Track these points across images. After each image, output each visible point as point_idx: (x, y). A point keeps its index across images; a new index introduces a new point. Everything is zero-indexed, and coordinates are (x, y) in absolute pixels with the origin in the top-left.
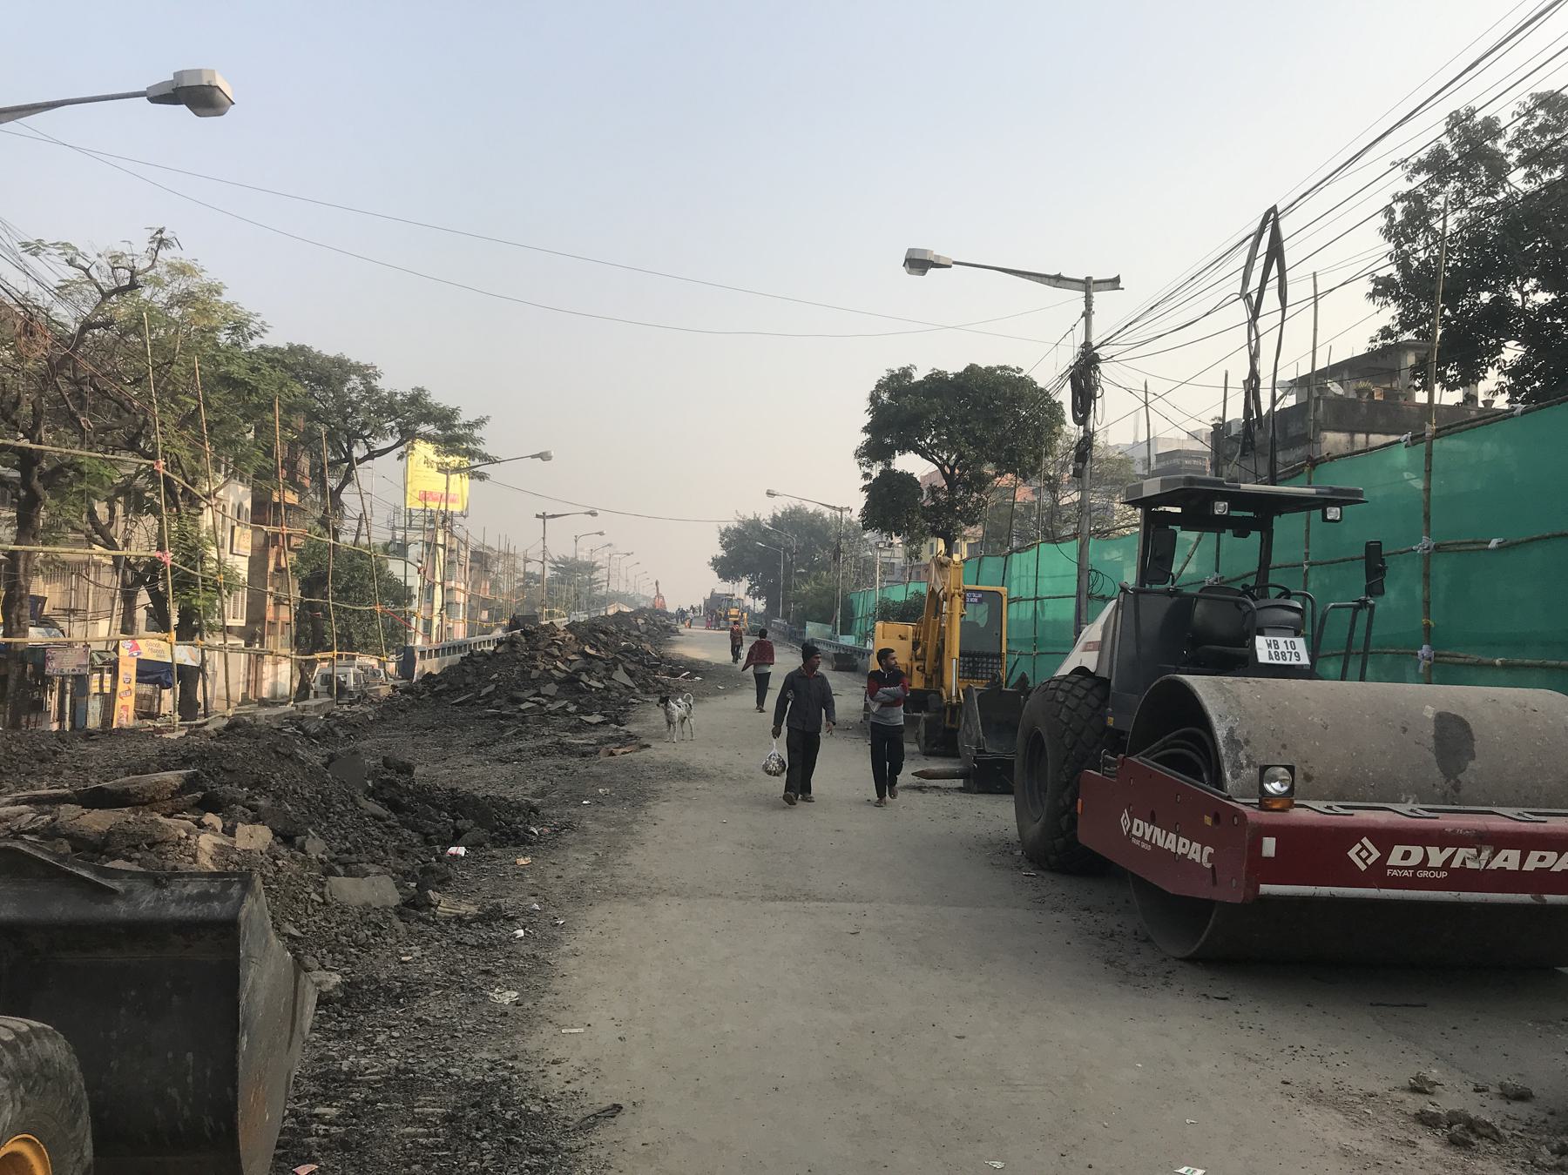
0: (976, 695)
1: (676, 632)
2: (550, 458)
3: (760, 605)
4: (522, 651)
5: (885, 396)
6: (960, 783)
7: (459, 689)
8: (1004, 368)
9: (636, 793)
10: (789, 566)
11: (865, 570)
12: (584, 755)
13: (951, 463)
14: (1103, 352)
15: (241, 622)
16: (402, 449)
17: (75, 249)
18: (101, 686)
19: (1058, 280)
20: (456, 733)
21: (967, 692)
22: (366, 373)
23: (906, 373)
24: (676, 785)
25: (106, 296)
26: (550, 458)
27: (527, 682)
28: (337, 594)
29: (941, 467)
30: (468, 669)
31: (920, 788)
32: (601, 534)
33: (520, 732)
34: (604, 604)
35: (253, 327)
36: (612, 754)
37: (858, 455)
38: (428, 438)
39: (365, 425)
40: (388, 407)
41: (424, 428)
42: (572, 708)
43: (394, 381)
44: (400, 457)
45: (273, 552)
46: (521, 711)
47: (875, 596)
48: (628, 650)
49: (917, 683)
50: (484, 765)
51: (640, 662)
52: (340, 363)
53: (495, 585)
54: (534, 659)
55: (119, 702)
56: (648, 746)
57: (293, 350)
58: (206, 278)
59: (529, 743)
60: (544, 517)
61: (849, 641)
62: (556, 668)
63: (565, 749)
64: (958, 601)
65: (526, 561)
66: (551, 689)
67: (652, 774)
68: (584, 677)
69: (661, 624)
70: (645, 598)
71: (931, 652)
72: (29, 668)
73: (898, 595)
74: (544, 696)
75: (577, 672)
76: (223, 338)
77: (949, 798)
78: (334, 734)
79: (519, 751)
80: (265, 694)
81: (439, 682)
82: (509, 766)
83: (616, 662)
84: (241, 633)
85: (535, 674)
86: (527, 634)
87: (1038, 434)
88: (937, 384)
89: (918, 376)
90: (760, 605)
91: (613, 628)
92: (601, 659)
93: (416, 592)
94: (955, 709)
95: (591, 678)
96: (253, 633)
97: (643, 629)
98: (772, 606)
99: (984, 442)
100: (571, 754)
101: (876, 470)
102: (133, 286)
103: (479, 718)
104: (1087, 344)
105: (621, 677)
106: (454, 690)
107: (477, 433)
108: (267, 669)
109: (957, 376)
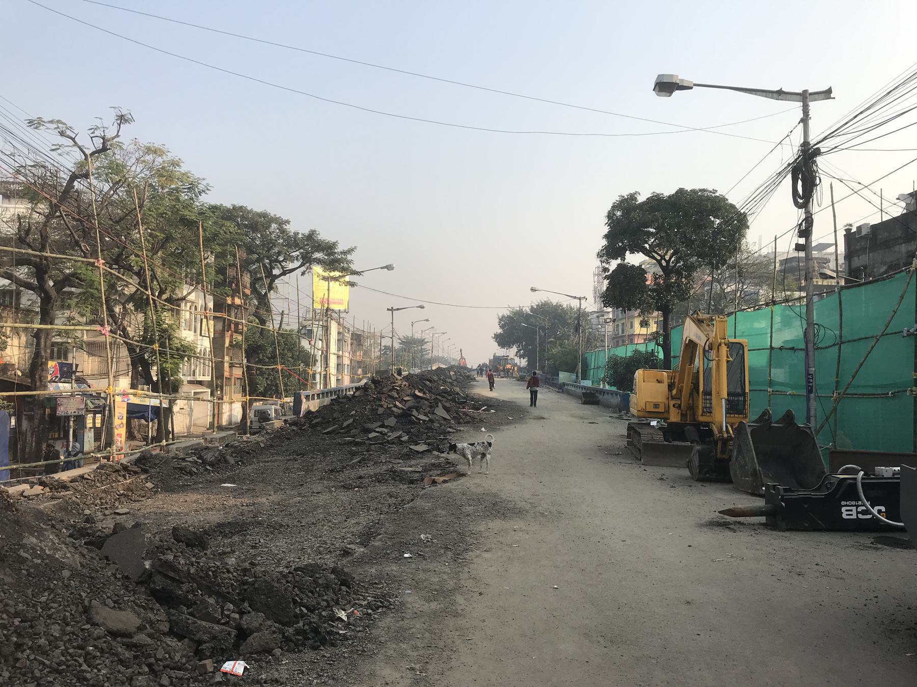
0: (749, 430)
1: (764, 418)
3: (523, 363)
5: (619, 213)
6: (763, 519)
7: (329, 422)
8: (703, 190)
9: (457, 546)
12: (412, 482)
13: (667, 258)
14: (823, 147)
16: (303, 269)
17: (65, 124)
18: (94, 423)
19: (780, 94)
20: (320, 457)
22: (281, 223)
23: (632, 197)
28: (269, 359)
29: (659, 262)
30: (336, 407)
31: (725, 525)
32: (427, 320)
33: (364, 459)
34: (430, 363)
35: (201, 187)
36: (434, 482)
37: (599, 255)
38: (319, 261)
39: (279, 253)
40: (293, 242)
41: (317, 255)
42: (405, 438)
43: (298, 226)
44: (303, 274)
45: (228, 334)
46: (369, 439)
48: (445, 391)
49: (674, 417)
50: (331, 492)
51: (454, 400)
52: (264, 215)
53: (366, 353)
54: (380, 400)
55: (116, 432)
56: (463, 475)
58: (169, 157)
59: (369, 470)
60: (392, 310)
61: (587, 383)
62: (395, 406)
63: (397, 477)
64: (724, 349)
65: (382, 337)
66: (392, 421)
67: (469, 509)
68: (415, 413)
69: (463, 375)
70: (454, 360)
72: (48, 411)
74: (386, 427)
75: (410, 409)
76: (184, 197)
78: (226, 461)
79: (361, 477)
80: (224, 422)
81: (316, 417)
82: (350, 493)
83: (437, 402)
84: (209, 385)
85: (381, 411)
86: (379, 385)
88: (656, 202)
89: (641, 199)
90: (523, 363)
91: (435, 378)
93: (318, 358)
94: (725, 442)
95: (419, 413)
96: (217, 385)
97: (454, 378)
98: (531, 363)
99: (693, 242)
100: (402, 480)
101: (614, 264)
102: (104, 149)
103: (340, 444)
104: (805, 144)
105: (440, 412)
106: (326, 423)
107: (349, 257)
108: (226, 408)
109: (669, 197)
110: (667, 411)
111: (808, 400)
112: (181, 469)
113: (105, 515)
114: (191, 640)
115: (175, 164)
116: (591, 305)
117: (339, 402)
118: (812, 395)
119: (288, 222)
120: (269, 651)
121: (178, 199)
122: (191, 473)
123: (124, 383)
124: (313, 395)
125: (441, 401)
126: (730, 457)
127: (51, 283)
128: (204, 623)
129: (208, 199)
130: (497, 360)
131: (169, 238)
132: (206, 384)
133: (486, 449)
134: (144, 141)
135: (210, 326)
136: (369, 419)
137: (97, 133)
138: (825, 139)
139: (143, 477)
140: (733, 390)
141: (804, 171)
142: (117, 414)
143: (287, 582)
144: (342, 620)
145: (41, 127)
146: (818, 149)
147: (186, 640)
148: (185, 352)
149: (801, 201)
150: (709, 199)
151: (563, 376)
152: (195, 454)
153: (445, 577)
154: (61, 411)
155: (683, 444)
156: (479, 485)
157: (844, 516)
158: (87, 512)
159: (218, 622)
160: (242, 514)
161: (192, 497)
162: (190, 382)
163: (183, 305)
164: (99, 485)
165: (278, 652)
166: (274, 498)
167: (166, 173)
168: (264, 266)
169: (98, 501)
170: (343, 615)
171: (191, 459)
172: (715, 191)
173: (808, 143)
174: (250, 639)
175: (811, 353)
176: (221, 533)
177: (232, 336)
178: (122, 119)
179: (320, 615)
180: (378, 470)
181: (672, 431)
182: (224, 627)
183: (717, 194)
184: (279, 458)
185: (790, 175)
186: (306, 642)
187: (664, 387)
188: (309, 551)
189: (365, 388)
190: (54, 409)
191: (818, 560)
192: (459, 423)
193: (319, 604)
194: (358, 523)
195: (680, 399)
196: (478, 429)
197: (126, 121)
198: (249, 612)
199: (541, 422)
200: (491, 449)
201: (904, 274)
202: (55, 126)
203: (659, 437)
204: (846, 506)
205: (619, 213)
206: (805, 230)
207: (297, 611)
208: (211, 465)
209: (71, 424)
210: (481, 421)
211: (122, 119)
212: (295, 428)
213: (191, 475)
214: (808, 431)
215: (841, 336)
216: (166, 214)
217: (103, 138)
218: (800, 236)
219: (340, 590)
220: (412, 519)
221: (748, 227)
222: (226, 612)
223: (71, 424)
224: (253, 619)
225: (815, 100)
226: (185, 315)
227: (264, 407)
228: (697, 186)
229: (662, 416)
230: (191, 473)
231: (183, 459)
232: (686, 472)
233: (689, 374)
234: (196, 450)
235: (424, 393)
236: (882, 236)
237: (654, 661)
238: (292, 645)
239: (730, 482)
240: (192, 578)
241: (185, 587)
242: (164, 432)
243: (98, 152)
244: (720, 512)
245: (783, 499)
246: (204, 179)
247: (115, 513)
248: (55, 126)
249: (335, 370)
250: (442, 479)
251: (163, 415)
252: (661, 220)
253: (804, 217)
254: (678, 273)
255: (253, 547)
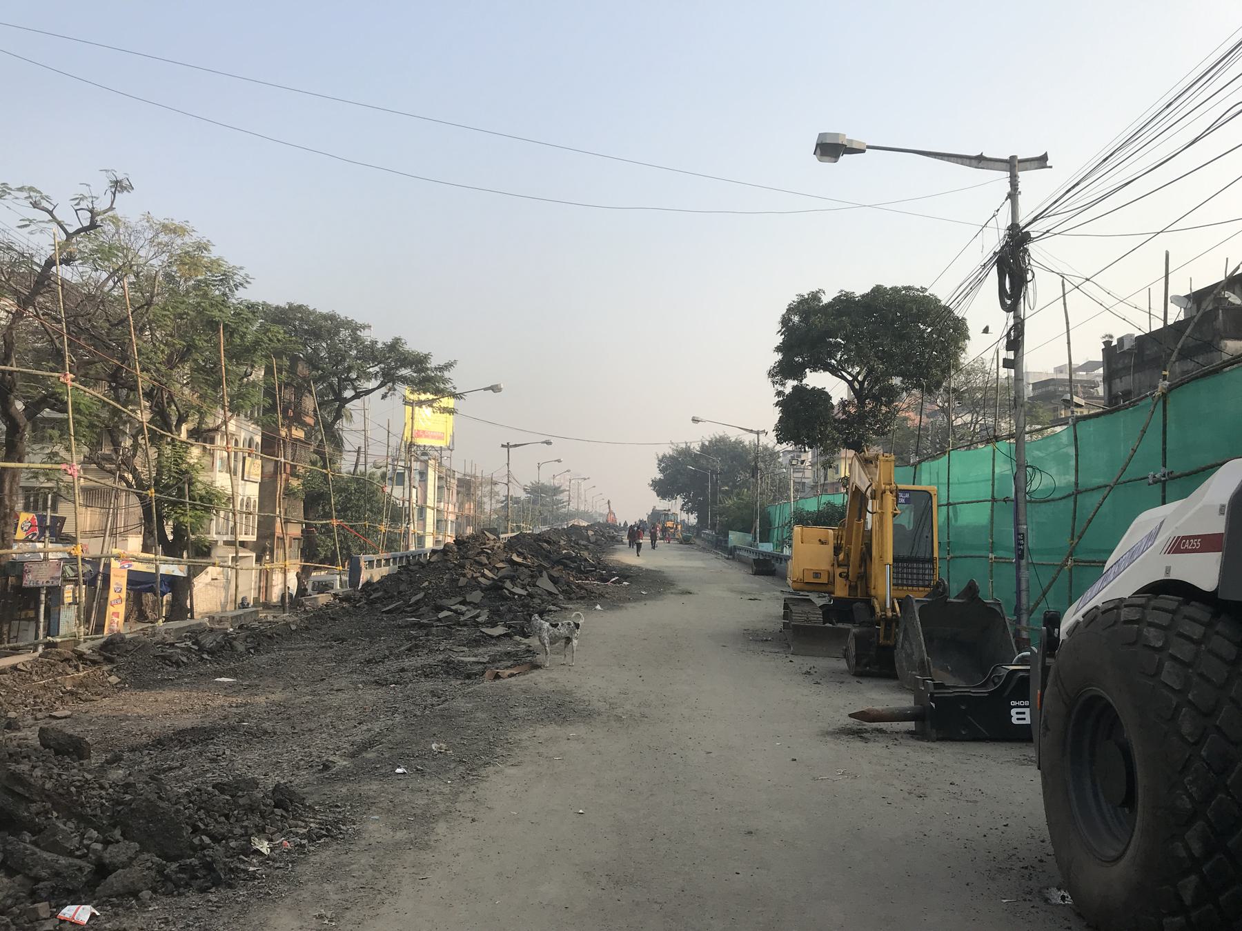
0: (916, 608)
2: (500, 390)
3: (692, 519)
4: (454, 560)
5: (796, 319)
6: (911, 725)
7: (392, 597)
8: (908, 288)
10: (715, 484)
11: (781, 489)
12: (469, 677)
14: (1034, 230)
15: (252, 538)
16: (383, 390)
19: (980, 161)
21: (904, 603)
22: (355, 328)
23: (815, 297)
24: (543, 732)
25: (69, 236)
26: (500, 390)
27: (457, 590)
28: (335, 510)
29: (850, 384)
30: (404, 577)
31: (858, 734)
32: (559, 461)
33: (416, 646)
35: (238, 279)
37: (772, 374)
38: (405, 380)
40: (370, 354)
41: (404, 372)
43: (379, 334)
44: (384, 397)
46: (439, 620)
47: (790, 508)
48: (568, 557)
49: (841, 591)
52: (332, 317)
53: (480, 505)
54: (463, 567)
55: (110, 610)
57: (292, 308)
60: (508, 446)
61: (767, 547)
62: (483, 575)
64: (890, 498)
66: (476, 596)
70: (601, 515)
71: (854, 558)
73: (811, 505)
75: (502, 579)
77: (901, 751)
78: (232, 648)
79: (403, 670)
81: (376, 590)
83: (541, 569)
85: (462, 582)
87: (945, 349)
88: (845, 303)
89: (826, 299)
90: (692, 519)
92: (527, 567)
94: (890, 623)
95: (515, 585)
96: (264, 547)
97: (593, 539)
101: (790, 384)
102: (93, 226)
103: (399, 626)
105: (545, 583)
107: (447, 374)
109: (863, 296)
110: (832, 582)
111: (1018, 568)
112: (164, 658)
113: (36, 719)
114: (27, 876)
115: (202, 247)
116: (770, 440)
117: (413, 569)
118: (1023, 562)
119: (364, 327)
120: (135, 894)
121: (205, 295)
122: (178, 664)
123: (134, 543)
124: (379, 561)
125: (546, 568)
126: (896, 641)
127: (19, 405)
128: (45, 855)
129: (244, 295)
130: (656, 515)
131: (190, 348)
132: (250, 546)
133: (572, 632)
134: (159, 216)
135: (254, 468)
136: (446, 593)
137: (83, 204)
138: (1035, 219)
139: (105, 668)
140: (905, 553)
141: (1012, 264)
142: (113, 586)
143: (190, 802)
144: (262, 854)
145: (7, 196)
146: (1028, 233)
147: (19, 878)
148: (209, 502)
149: (1009, 302)
150: (915, 300)
151: (734, 538)
152: (190, 638)
153: (438, 798)
154: (29, 581)
155: (839, 627)
156: (552, 680)
157: (1014, 721)
158: (12, 714)
159: (70, 854)
160: (225, 718)
161: (169, 694)
162: (227, 543)
163: (218, 438)
164: (35, 678)
165: (146, 894)
166: (277, 696)
167: (191, 260)
168: (331, 385)
169: (31, 701)
170: (264, 847)
171: (183, 645)
172: (924, 290)
173: (1018, 225)
174: (111, 878)
175: (1021, 506)
176: (180, 742)
177: (287, 480)
178: (118, 186)
179: (227, 847)
180: (431, 661)
181: (839, 611)
182: (78, 862)
183: (927, 294)
184: (312, 644)
185: (995, 267)
186: (193, 882)
187: (829, 549)
188: (285, 765)
189: (446, 551)
190: (20, 578)
191: (957, 780)
192: (570, 599)
193: (231, 831)
194: (369, 730)
195: (848, 566)
196: (591, 606)
197: (123, 189)
198: (118, 842)
199: (685, 598)
200: (578, 632)
201: (1149, 400)
202: (25, 194)
203: (817, 617)
204: (1017, 707)
205: (796, 319)
206: (1015, 341)
207: (196, 841)
208: (211, 652)
209: (43, 597)
210: (601, 596)
211: (118, 186)
212: (345, 605)
213: (179, 666)
214: (997, 608)
215: (1076, 484)
216: (188, 314)
217: (91, 211)
218: (1008, 349)
219: (273, 812)
220: (436, 724)
221: (968, 338)
222: (85, 842)
223: (43, 597)
224: (121, 851)
225: (1026, 169)
226: (220, 455)
227: (329, 578)
228: (900, 283)
229: (824, 588)
230: (178, 664)
231: (172, 645)
232: (843, 665)
233: (857, 535)
234: (193, 632)
235: (525, 558)
236: (1151, 351)
237: (657, 907)
238: (170, 886)
239: (895, 677)
240: (47, 796)
241: (34, 808)
242: (180, 609)
243: (84, 229)
244: (850, 716)
245: (932, 699)
246: (241, 268)
247: (51, 716)
248: (25, 194)
249: (432, 526)
250: (508, 672)
251: (179, 587)
252: (849, 327)
253: (1011, 322)
254: (876, 398)
255: (213, 761)
